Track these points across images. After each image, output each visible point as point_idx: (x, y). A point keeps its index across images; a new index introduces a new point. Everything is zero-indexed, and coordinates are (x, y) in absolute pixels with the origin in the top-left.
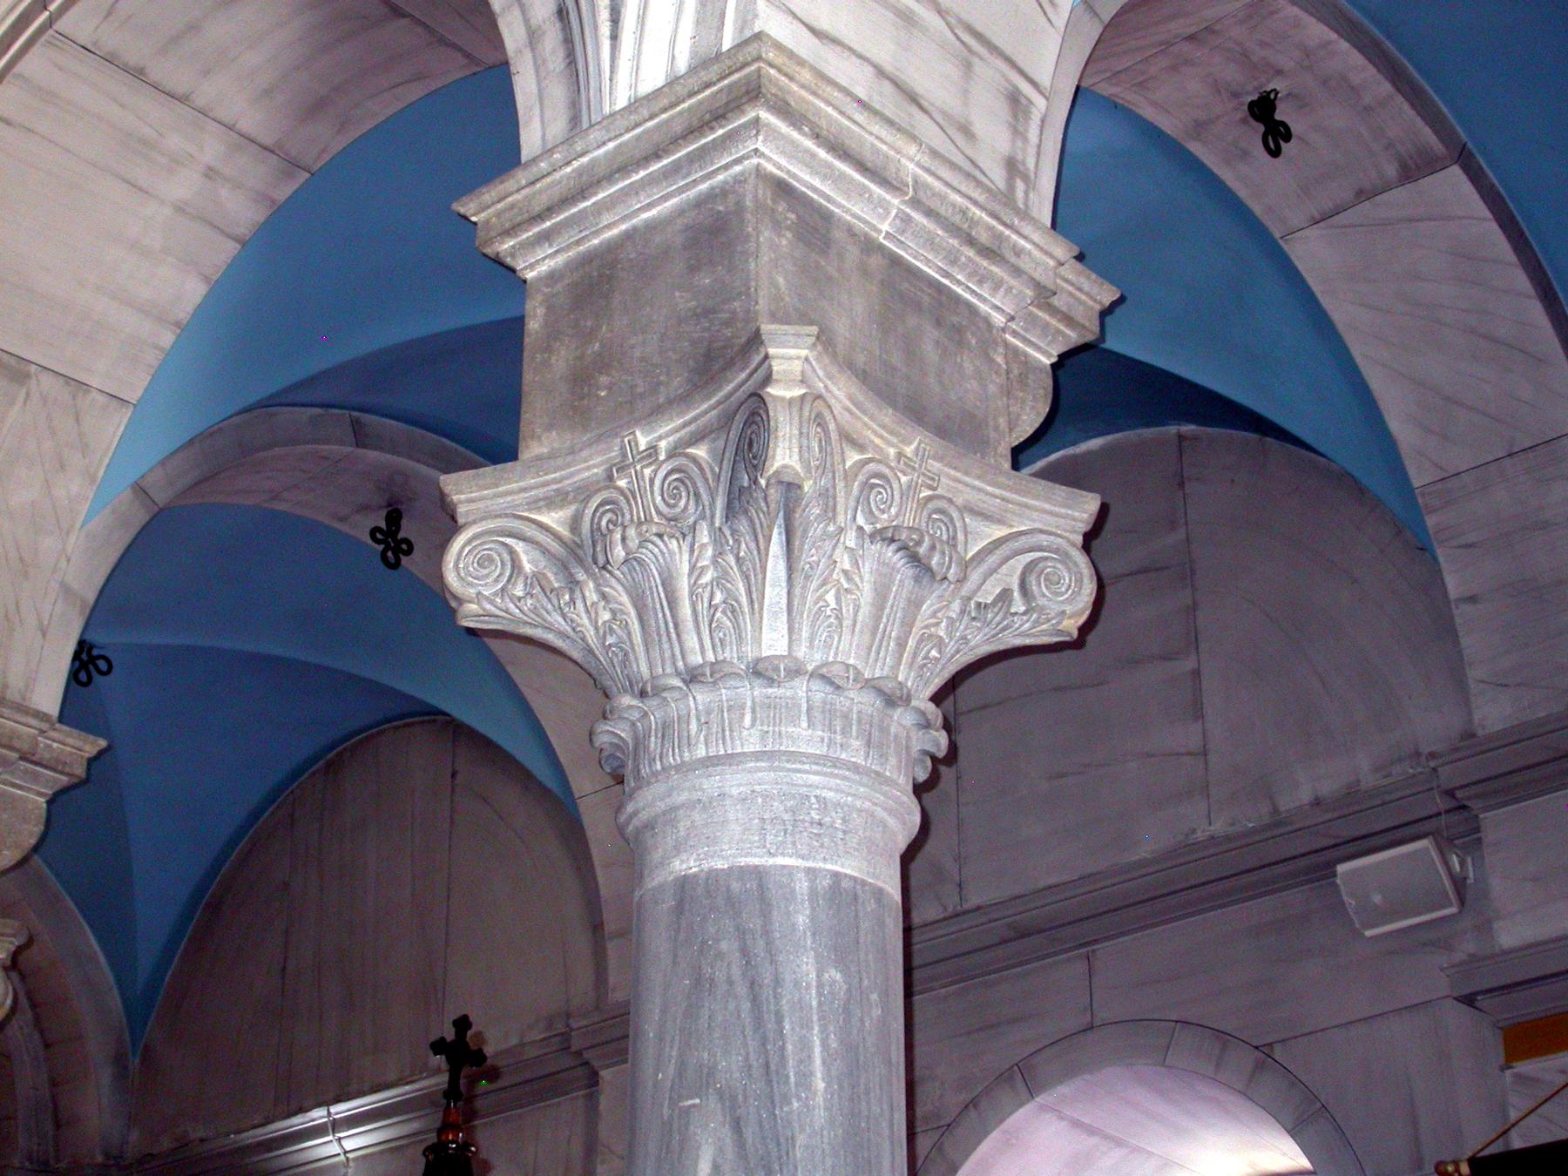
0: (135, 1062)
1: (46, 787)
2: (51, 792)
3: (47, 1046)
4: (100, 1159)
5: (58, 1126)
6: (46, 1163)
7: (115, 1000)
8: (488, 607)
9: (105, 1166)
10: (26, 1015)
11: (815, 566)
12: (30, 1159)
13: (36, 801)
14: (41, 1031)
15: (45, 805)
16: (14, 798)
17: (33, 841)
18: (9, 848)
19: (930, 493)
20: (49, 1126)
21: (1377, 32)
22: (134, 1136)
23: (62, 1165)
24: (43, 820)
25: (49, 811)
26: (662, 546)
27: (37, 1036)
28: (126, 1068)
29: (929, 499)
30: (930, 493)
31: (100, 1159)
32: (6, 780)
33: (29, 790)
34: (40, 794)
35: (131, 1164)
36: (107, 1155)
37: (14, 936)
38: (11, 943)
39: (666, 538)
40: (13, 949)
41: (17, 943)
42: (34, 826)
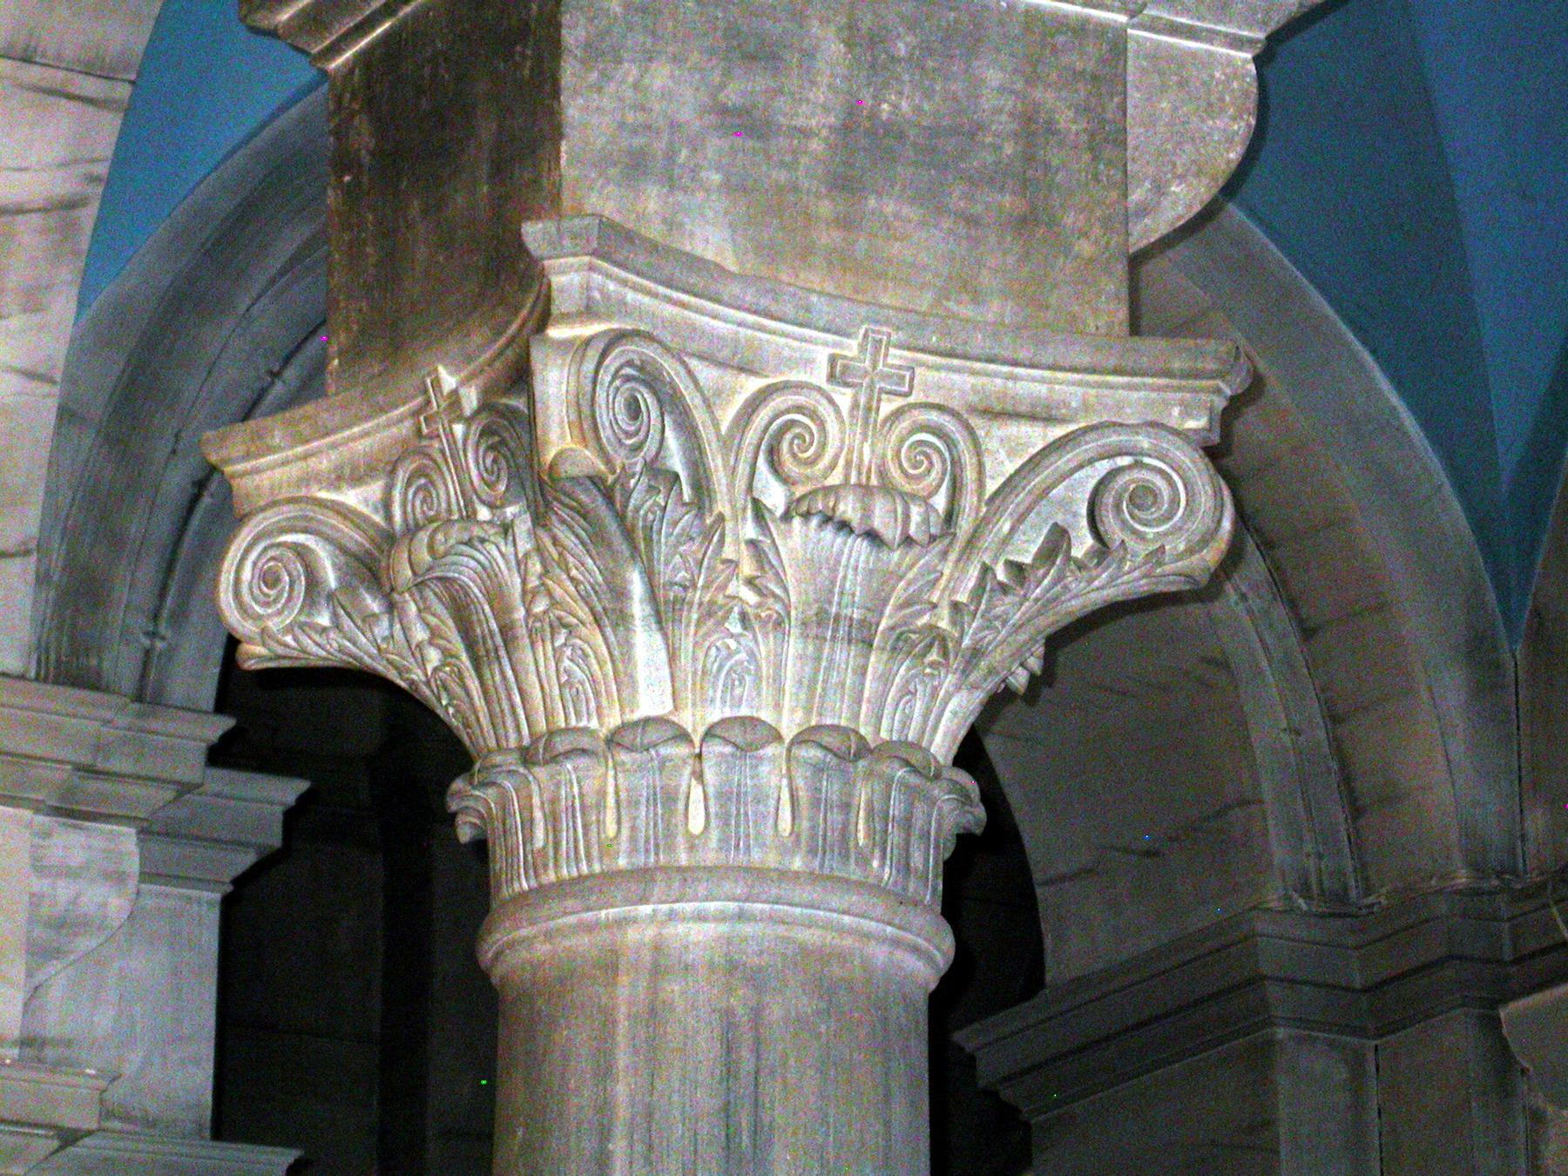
0: (1514, 654)
1: (1250, 22)
2: (1261, 36)
3: (1308, 633)
4: (1462, 878)
5: (1356, 811)
6: (1341, 897)
7: (1454, 514)
8: (274, 645)
9: (1479, 893)
10: (1255, 566)
11: (556, 624)
12: (1305, 890)
13: (1230, 61)
14: (1293, 605)
15: (1252, 68)
16: (1181, 60)
17: (1234, 155)
18: (1182, 178)
19: (898, 402)
20: (1338, 815)
21: (402, 409)
22: (1537, 822)
23: (1380, 898)
24: (1252, 103)
25: (1260, 76)
26: (478, 555)
27: (1280, 612)
28: (1498, 666)
29: (897, 414)
30: (898, 402)
31: (1462, 878)
32: (1154, 19)
33: (1210, 37)
34: (1236, 42)
35: (1542, 887)
36: (1478, 868)
37: (1219, 375)
38: (1218, 391)
39: (476, 543)
40: (1220, 403)
41: (1228, 392)
42: (1234, 119)
